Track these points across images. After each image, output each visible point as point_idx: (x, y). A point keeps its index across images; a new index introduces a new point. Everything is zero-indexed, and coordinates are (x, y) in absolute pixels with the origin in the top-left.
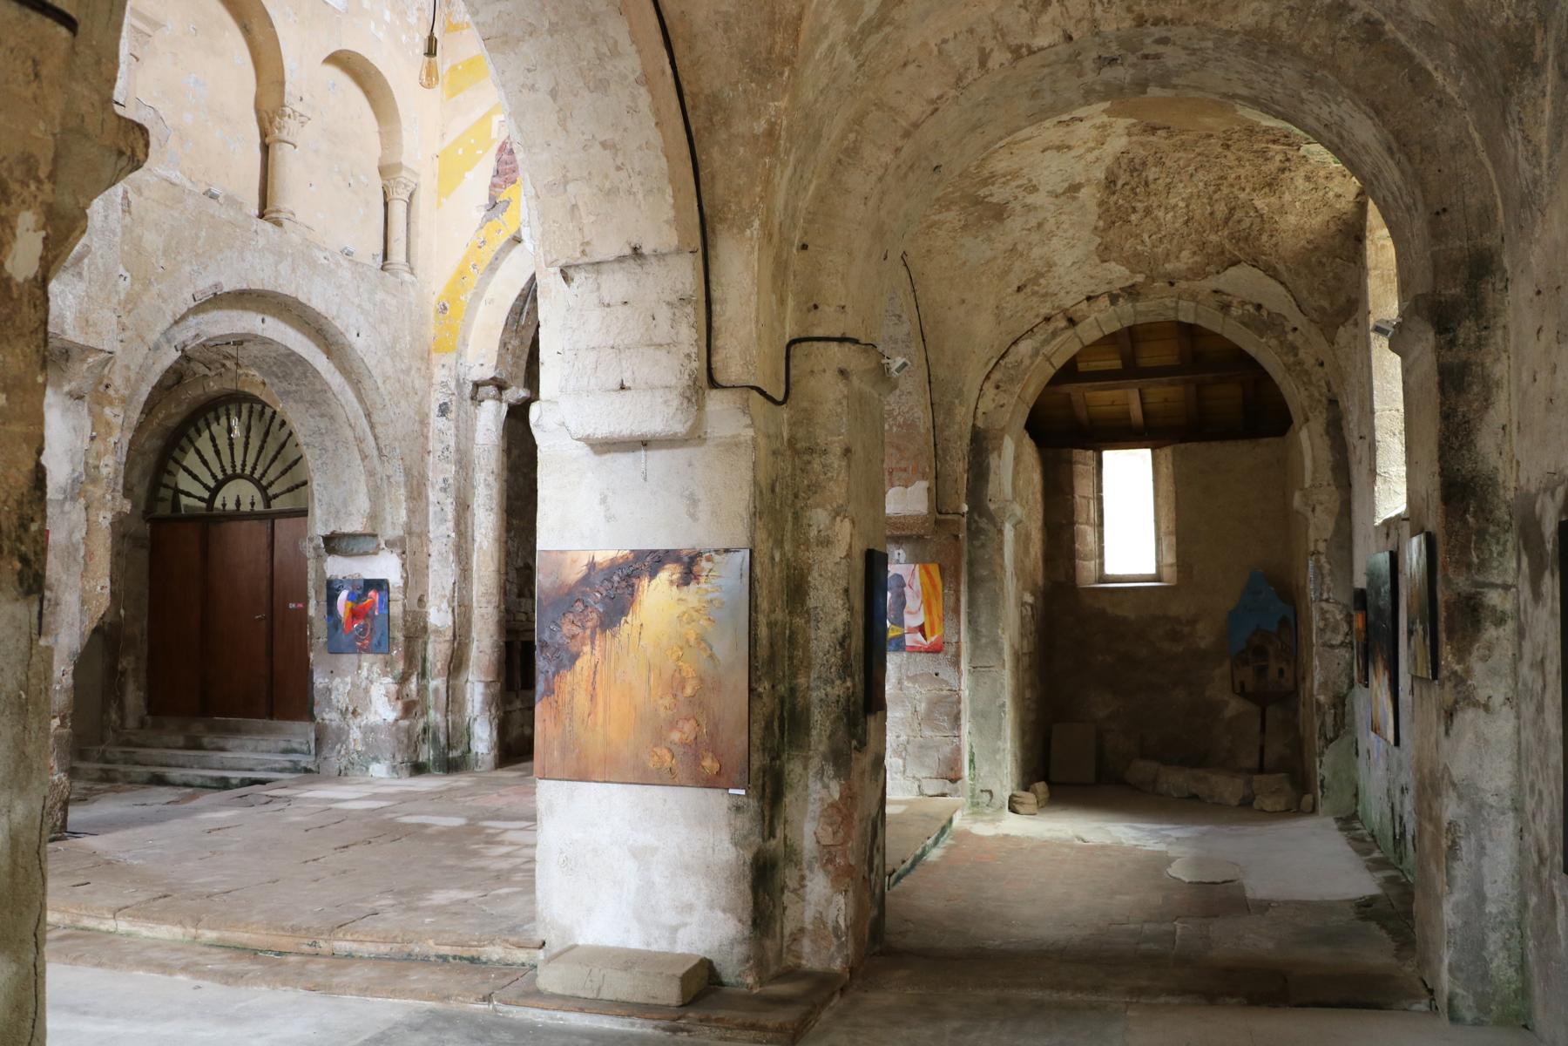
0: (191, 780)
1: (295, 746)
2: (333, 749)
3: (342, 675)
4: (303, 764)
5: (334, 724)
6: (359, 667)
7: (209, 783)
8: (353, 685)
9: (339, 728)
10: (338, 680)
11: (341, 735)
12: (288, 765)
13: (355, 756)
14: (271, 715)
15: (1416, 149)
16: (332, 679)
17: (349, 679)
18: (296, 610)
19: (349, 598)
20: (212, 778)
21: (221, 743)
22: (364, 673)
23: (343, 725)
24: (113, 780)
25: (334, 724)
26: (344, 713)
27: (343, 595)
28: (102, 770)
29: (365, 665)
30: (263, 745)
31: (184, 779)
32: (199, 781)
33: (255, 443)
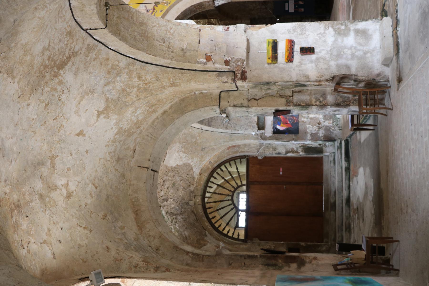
0: (347, 186)
1: (332, 159)
2: (332, 133)
3: (306, 129)
4: (339, 145)
5: (323, 132)
6: (303, 122)
7: (348, 177)
8: (309, 124)
9: (325, 130)
10: (308, 130)
11: (327, 129)
12: (339, 151)
13: (334, 123)
14: (320, 183)
15: (53, 244)
16: (308, 133)
17: (308, 126)
18: (283, 171)
19: (279, 125)
20: (346, 175)
21: (333, 193)
22: (305, 119)
23: (324, 128)
24: (350, 225)
25: (323, 132)
26: (320, 128)
27: (278, 127)
28: (346, 231)
29: (303, 119)
30: (333, 173)
31: (347, 189)
32: (347, 181)
33: (222, 212)
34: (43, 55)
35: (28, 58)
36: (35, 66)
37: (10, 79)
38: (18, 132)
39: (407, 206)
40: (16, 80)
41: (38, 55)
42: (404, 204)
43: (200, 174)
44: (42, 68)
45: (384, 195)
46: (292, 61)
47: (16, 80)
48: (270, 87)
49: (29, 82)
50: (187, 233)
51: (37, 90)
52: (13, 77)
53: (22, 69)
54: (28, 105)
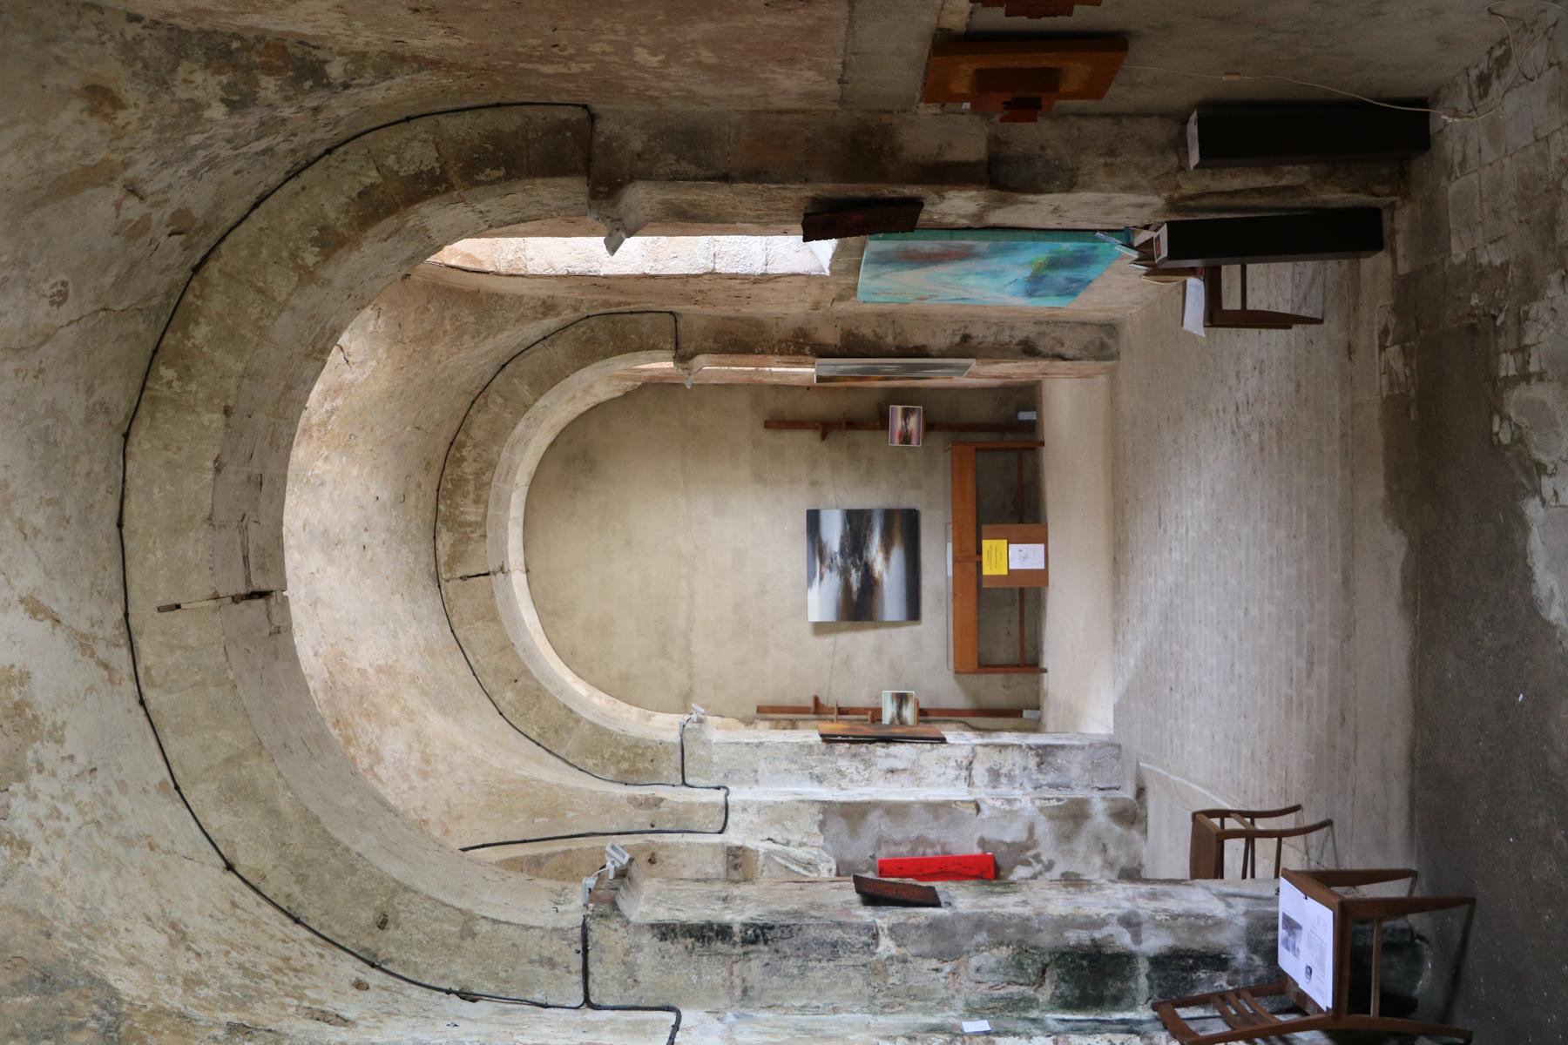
34: (369, 751)
35: (395, 712)
36: (363, 722)
37: (382, 662)
38: (303, 591)
39: (1262, 449)
40: (371, 671)
41: (379, 738)
42: (1270, 454)
43: (1036, 948)
44: (350, 732)
45: (1380, 492)
46: (1299, 927)
47: (371, 671)
48: (1457, 158)
49: (347, 690)
50: (224, 79)
51: (325, 691)
52: (380, 670)
53: (382, 691)
54: (316, 654)
